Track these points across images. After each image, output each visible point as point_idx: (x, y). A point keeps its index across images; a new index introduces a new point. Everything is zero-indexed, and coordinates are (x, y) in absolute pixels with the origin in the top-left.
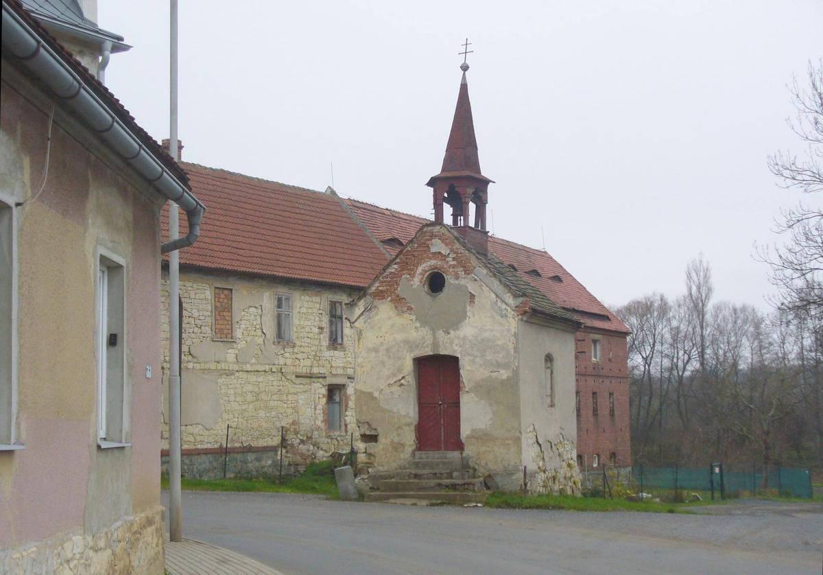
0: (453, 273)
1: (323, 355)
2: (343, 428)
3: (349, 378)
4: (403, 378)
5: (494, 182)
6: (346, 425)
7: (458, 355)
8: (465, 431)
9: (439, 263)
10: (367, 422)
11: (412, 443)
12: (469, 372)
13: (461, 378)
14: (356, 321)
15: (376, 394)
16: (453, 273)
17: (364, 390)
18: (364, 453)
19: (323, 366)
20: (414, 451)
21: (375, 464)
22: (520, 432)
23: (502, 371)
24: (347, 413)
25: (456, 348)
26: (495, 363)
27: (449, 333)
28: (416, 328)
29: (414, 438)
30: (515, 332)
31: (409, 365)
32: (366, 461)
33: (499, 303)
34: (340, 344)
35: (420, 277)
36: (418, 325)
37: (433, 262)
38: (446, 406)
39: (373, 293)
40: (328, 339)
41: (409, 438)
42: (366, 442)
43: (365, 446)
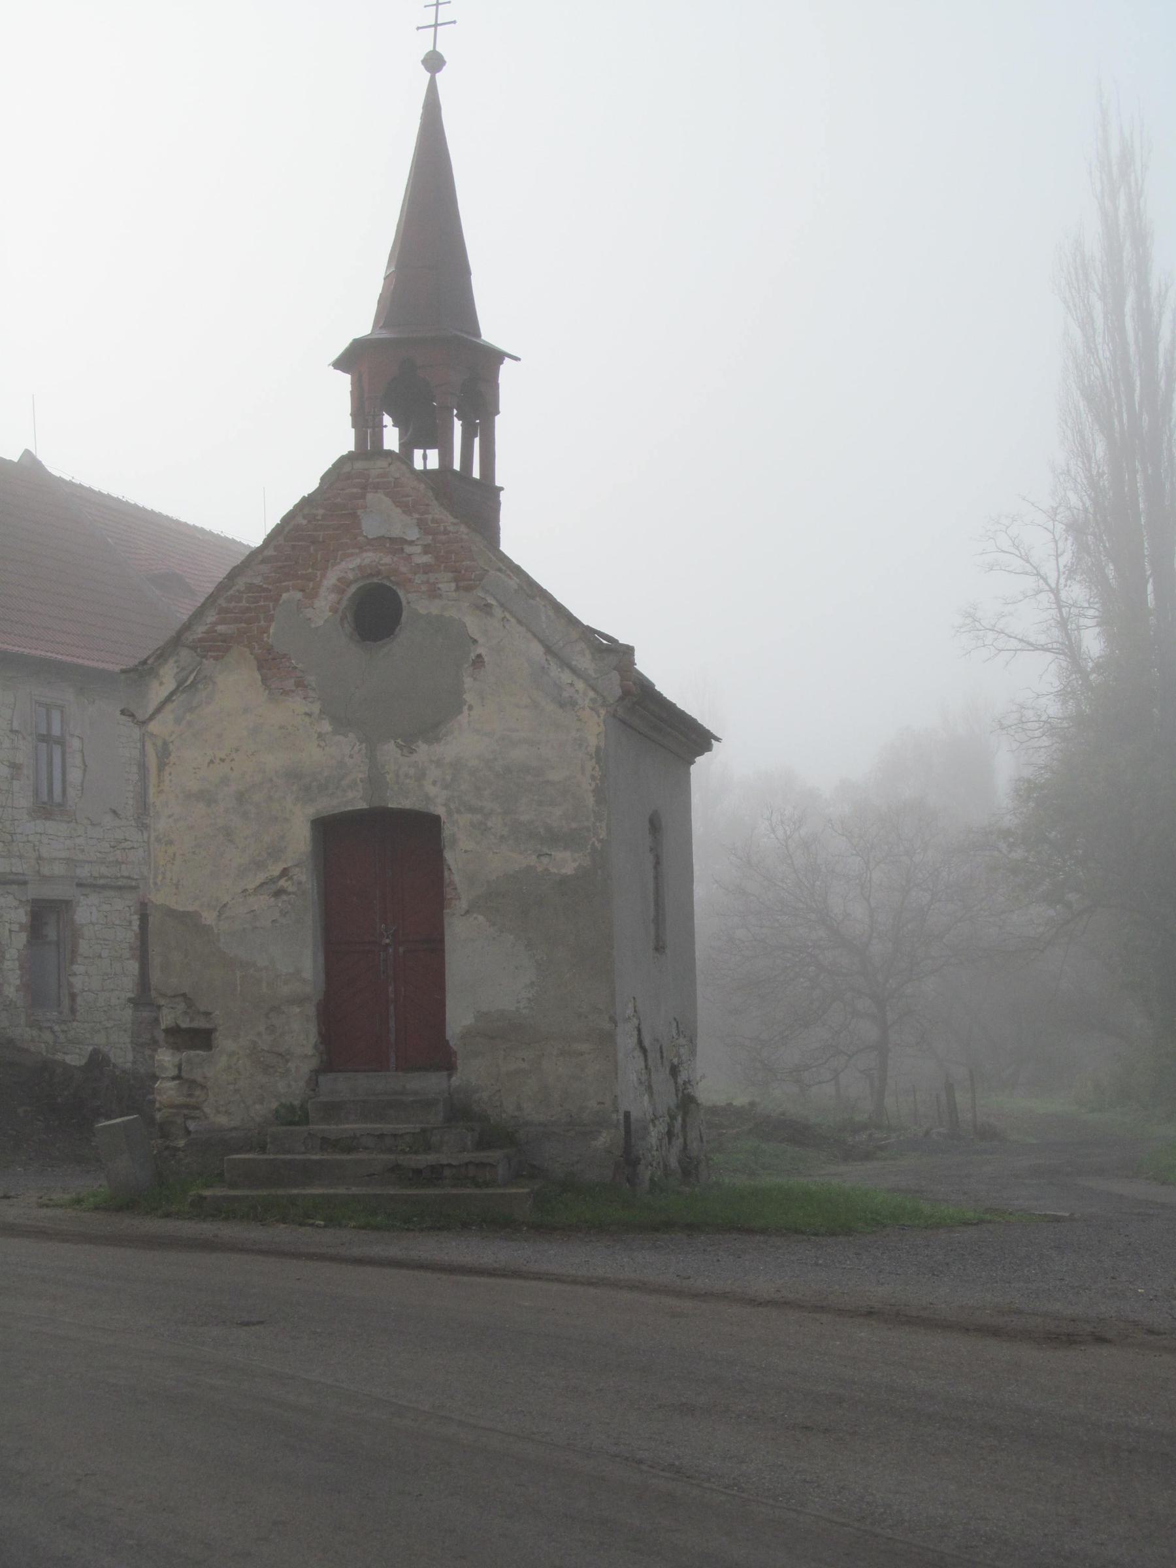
0: (424, 588)
1: (19, 830)
2: (66, 1002)
3: (79, 885)
4: (285, 872)
5: (516, 359)
6: (73, 997)
7: (440, 811)
8: (459, 1018)
9: (387, 559)
10: (184, 995)
11: (309, 1051)
12: (469, 856)
13: (446, 874)
14: (152, 717)
15: (209, 918)
16: (424, 588)
17: (175, 907)
18: (173, 1078)
19: (21, 857)
20: (317, 1072)
21: (207, 1110)
22: (613, 1020)
23: (560, 855)
24: (75, 967)
25: (432, 790)
26: (542, 830)
27: (412, 751)
28: (320, 735)
29: (313, 1038)
30: (598, 749)
31: (299, 837)
32: (181, 1100)
33: (555, 670)
34: (60, 805)
35: (333, 597)
36: (326, 727)
37: (369, 557)
38: (401, 950)
39: (201, 640)
40: (405, 614)
41: (301, 1035)
42: (177, 1048)
43: (177, 1060)
